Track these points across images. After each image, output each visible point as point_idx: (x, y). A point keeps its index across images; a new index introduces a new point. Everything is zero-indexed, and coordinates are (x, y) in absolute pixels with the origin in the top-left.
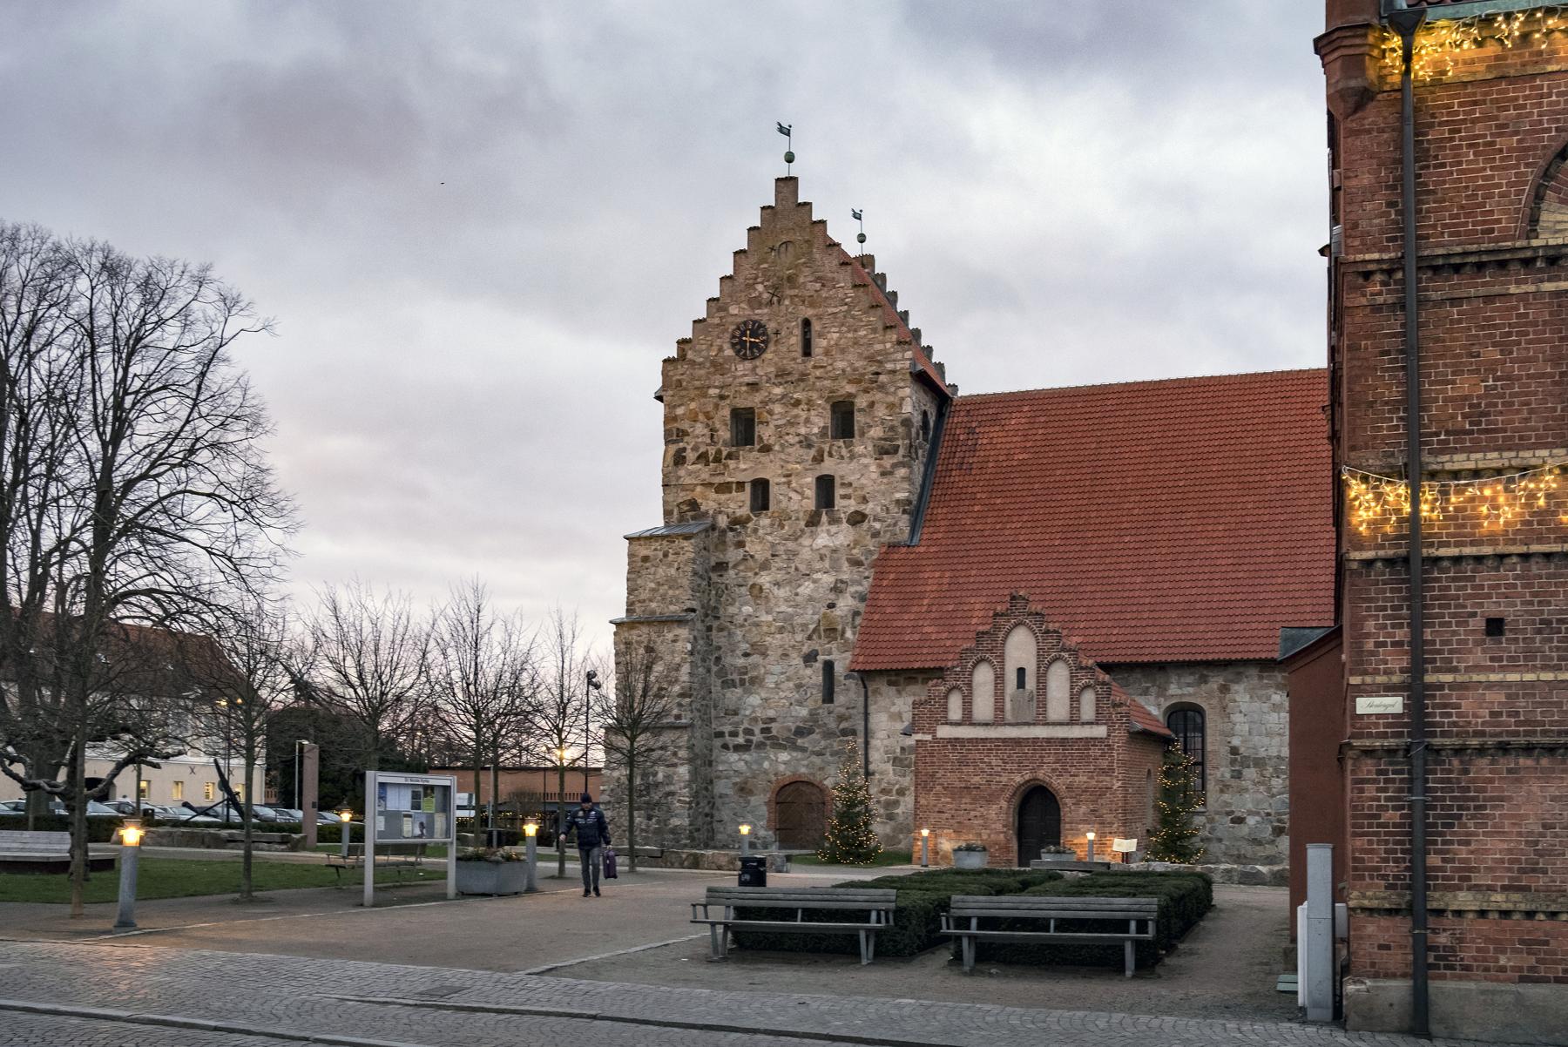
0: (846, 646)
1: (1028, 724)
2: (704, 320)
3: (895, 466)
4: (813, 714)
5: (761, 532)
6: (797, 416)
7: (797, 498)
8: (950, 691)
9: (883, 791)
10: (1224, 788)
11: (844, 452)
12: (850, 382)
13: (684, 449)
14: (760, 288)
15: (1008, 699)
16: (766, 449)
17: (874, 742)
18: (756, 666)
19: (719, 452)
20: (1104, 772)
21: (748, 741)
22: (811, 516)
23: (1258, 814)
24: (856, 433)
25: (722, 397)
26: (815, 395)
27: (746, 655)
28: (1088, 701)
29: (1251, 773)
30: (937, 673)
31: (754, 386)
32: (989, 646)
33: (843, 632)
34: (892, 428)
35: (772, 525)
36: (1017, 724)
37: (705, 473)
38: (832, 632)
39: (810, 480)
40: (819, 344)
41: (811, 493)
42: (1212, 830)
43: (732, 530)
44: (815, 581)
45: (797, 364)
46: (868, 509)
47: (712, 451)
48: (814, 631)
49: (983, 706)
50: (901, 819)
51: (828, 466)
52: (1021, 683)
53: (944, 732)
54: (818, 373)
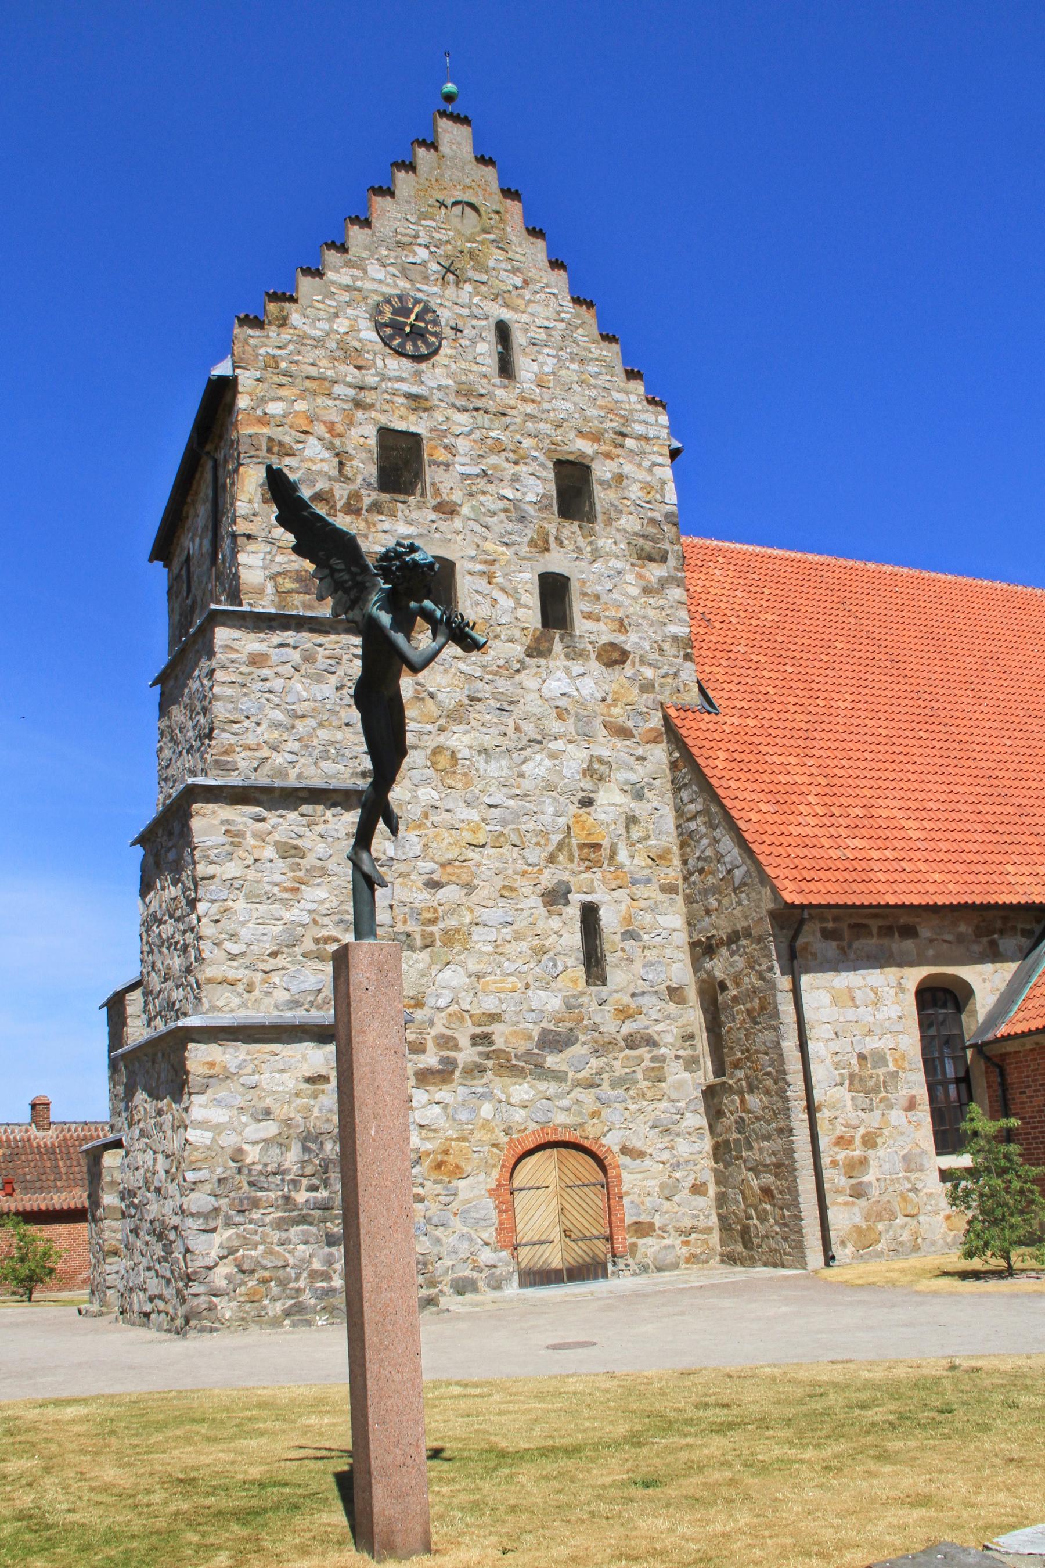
11: (581, 542)
12: (580, 433)
19: (355, 496)
21: (447, 1061)
22: (537, 640)
24: (600, 517)
33: (613, 854)
40: (526, 368)
41: (532, 599)
44: (553, 756)
46: (630, 641)
48: (560, 846)
50: (875, 1192)
51: (557, 562)
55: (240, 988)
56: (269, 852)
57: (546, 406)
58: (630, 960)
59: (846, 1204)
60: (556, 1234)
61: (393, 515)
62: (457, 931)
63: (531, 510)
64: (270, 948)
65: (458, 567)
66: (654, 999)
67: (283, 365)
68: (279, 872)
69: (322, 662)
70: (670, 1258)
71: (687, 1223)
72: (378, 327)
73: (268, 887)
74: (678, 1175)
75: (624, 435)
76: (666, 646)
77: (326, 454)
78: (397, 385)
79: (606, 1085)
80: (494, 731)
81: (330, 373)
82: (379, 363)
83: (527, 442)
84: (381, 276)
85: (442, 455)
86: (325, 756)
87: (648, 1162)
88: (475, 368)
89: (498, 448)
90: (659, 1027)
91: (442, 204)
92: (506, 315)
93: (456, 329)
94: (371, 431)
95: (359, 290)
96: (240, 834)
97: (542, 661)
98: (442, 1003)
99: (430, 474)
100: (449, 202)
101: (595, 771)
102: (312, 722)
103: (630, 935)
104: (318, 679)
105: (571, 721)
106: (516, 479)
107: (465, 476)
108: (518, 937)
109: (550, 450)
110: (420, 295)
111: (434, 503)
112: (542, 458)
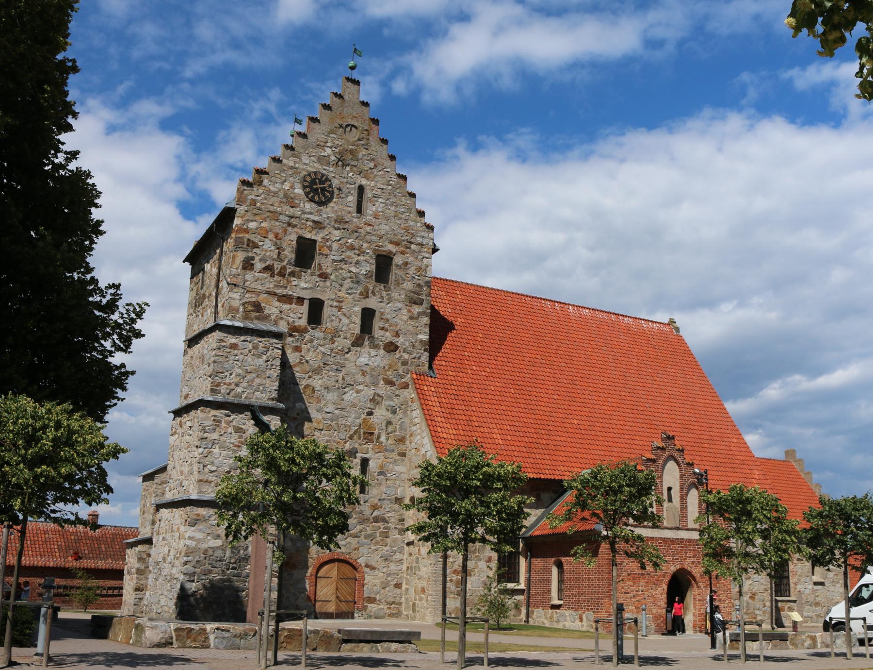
12: (391, 242)
22: (357, 339)
33: (379, 437)
40: (370, 209)
44: (358, 392)
46: (400, 341)
47: (277, 266)
48: (356, 432)
51: (372, 303)
55: (213, 484)
56: (230, 430)
57: (376, 227)
58: (380, 484)
59: (454, 598)
60: (333, 598)
61: (299, 277)
63: (362, 277)
64: (227, 469)
65: (325, 304)
66: (389, 502)
67: (258, 204)
69: (261, 349)
70: (382, 614)
71: (391, 600)
72: (304, 187)
73: (228, 444)
74: (389, 579)
75: (411, 243)
76: (416, 344)
77: (273, 248)
78: (308, 216)
79: (362, 537)
80: (333, 379)
81: (279, 209)
82: (302, 205)
83: (365, 245)
84: (307, 162)
85: (326, 251)
86: (257, 390)
87: (377, 572)
88: (346, 208)
89: (352, 248)
90: (389, 515)
91: (341, 126)
92: (364, 182)
93: (340, 189)
94: (294, 237)
95: (296, 168)
97: (358, 349)
100: (344, 125)
101: (375, 400)
102: (254, 375)
103: (381, 473)
104: (259, 356)
106: (357, 263)
107: (334, 261)
109: (375, 250)
110: (324, 172)
111: (318, 273)
112: (371, 253)
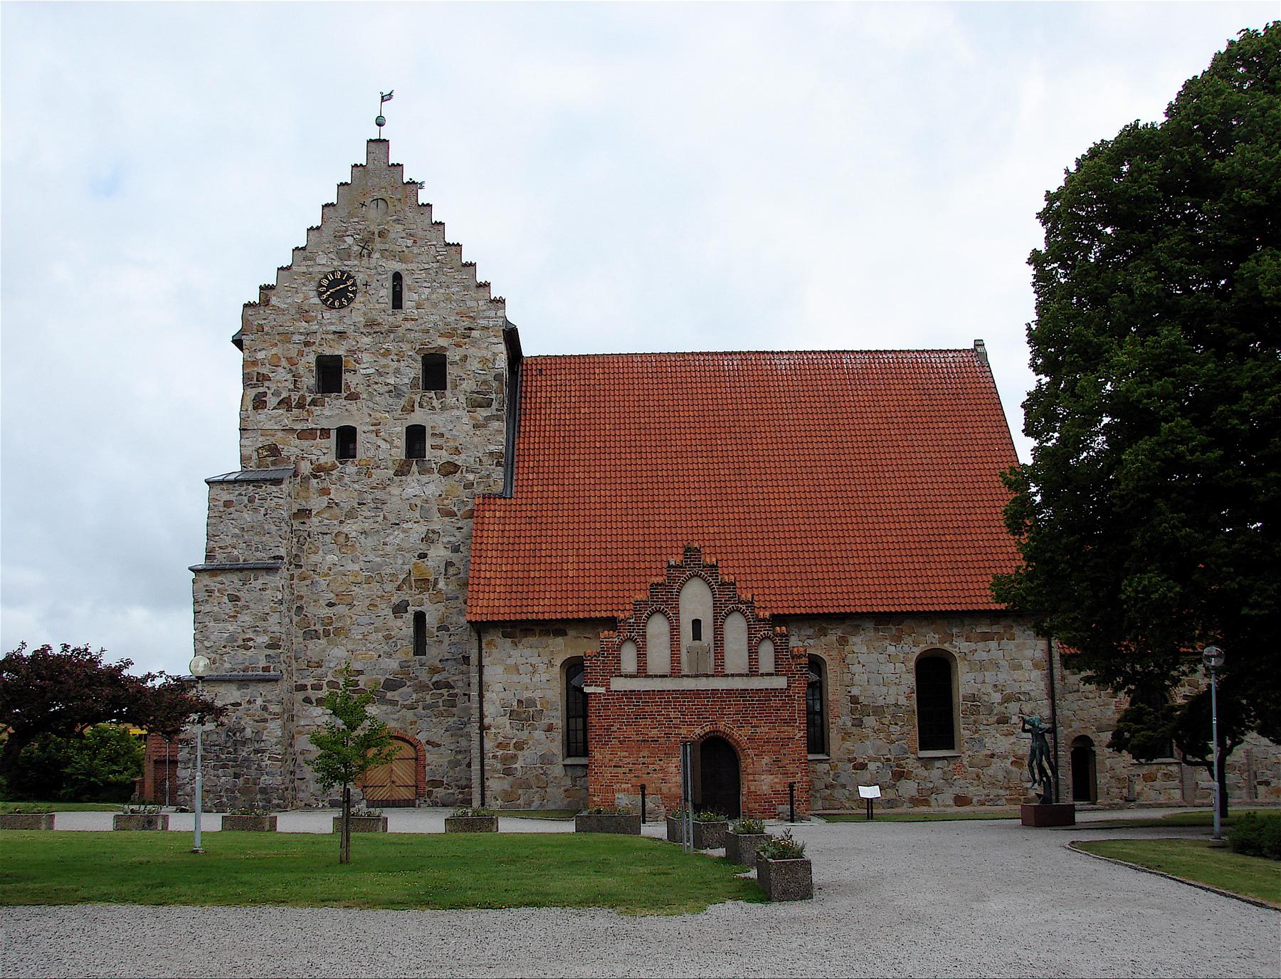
0: (439, 597)
1: (707, 676)
2: (288, 268)
3: (487, 418)
4: (404, 666)
5: (346, 479)
6: (385, 366)
7: (382, 445)
8: (623, 642)
9: (499, 745)
10: (846, 735)
11: (435, 403)
12: (441, 335)
13: (265, 394)
14: (349, 240)
15: (684, 651)
16: (353, 397)
17: (487, 695)
18: (341, 617)
19: (303, 397)
20: (786, 722)
22: (401, 466)
23: (879, 759)
24: (449, 386)
25: (307, 344)
26: (406, 347)
27: (330, 605)
28: (767, 653)
29: (870, 721)
30: (611, 623)
31: (341, 334)
32: (664, 599)
33: (436, 583)
34: (485, 382)
35: (359, 473)
36: (697, 676)
37: (287, 418)
38: (424, 583)
39: (400, 430)
40: (409, 298)
41: (401, 443)
42: (837, 776)
43: (316, 477)
44: (404, 531)
45: (388, 319)
46: (459, 460)
47: (295, 397)
49: (659, 657)
50: (519, 774)
51: (418, 418)
52: (697, 635)
53: (618, 684)
54: (408, 325)
56: (226, 599)
62: (342, 628)
68: (229, 607)
76: (484, 459)
86: (257, 550)
96: (211, 591)
98: (332, 665)
99: (346, 377)
105: (418, 510)
108: (377, 630)
